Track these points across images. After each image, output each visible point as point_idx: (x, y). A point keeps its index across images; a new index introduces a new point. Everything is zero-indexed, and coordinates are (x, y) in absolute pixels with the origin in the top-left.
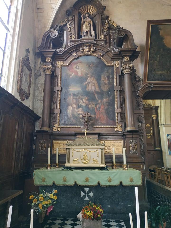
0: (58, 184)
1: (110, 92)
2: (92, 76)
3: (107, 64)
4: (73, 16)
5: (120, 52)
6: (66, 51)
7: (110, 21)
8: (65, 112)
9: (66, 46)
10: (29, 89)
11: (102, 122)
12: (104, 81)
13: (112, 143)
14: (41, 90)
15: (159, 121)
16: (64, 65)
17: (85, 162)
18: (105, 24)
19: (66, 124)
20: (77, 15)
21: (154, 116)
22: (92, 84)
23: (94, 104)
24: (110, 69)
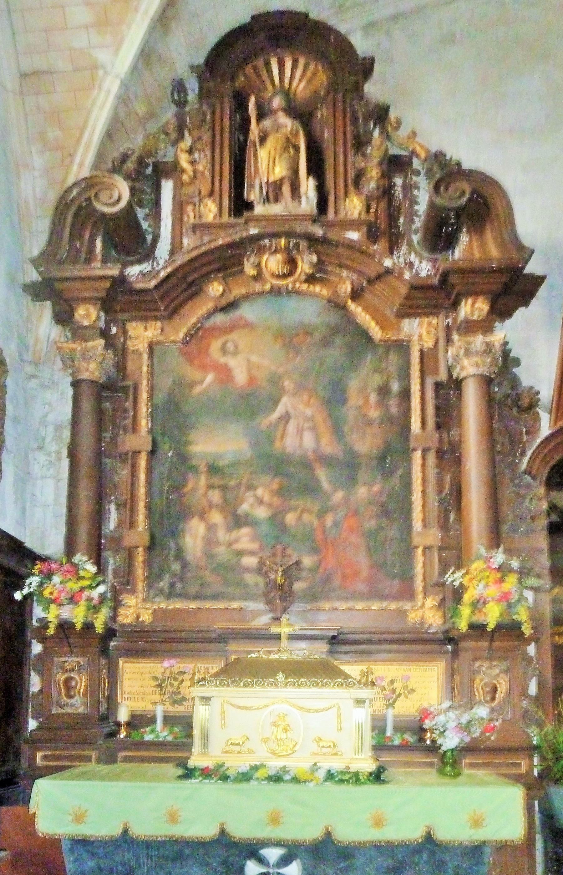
1: (394, 453)
2: (300, 388)
3: (376, 333)
5: (445, 277)
9: (172, 253)
10: (105, 278)
14: (59, 453)
20: (226, 100)
23: (310, 512)
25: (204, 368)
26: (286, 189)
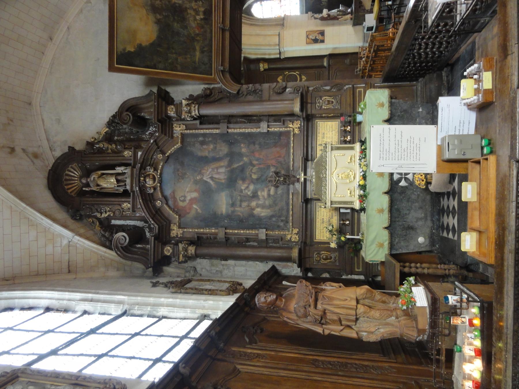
0: (387, 221)
2: (200, 173)
3: (179, 145)
4: (84, 206)
6: (152, 219)
7: (95, 139)
11: (283, 156)
12: (209, 152)
13: (321, 139)
14: (223, 265)
15: (272, 57)
16: (177, 224)
17: (352, 177)
18: (102, 149)
19: (286, 218)
21: (262, 67)
23: (252, 170)
25: (190, 209)
26: (120, 178)
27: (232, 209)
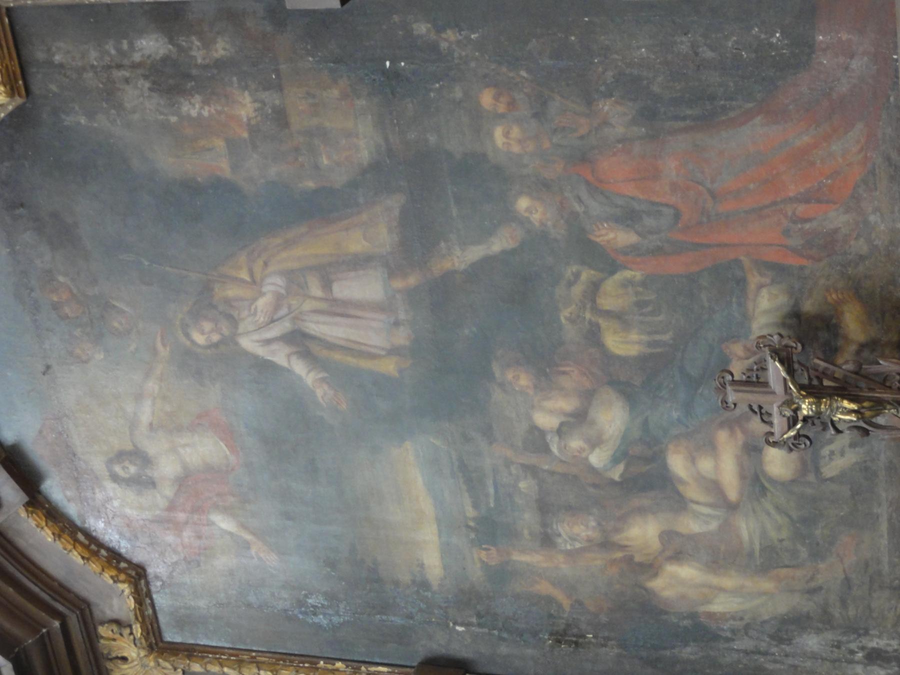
2: (205, 303)
8: (736, 645)
12: (233, 145)
22: (308, 306)
23: (595, 288)
24: (58, 58)
27: (492, 557)
